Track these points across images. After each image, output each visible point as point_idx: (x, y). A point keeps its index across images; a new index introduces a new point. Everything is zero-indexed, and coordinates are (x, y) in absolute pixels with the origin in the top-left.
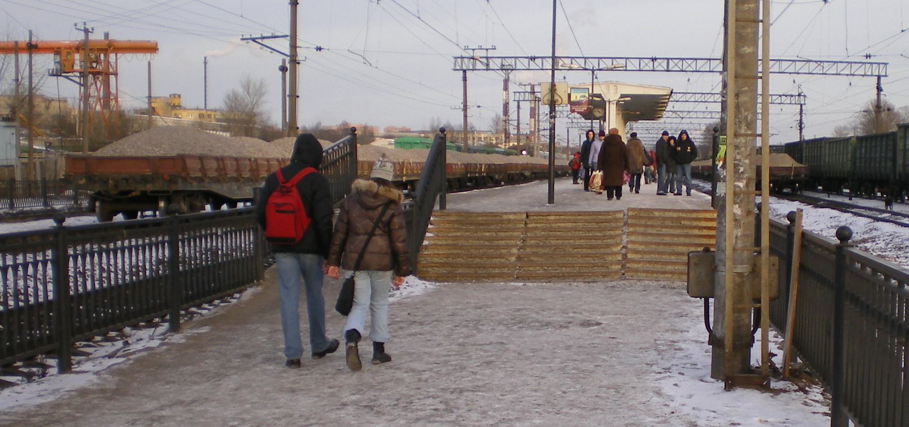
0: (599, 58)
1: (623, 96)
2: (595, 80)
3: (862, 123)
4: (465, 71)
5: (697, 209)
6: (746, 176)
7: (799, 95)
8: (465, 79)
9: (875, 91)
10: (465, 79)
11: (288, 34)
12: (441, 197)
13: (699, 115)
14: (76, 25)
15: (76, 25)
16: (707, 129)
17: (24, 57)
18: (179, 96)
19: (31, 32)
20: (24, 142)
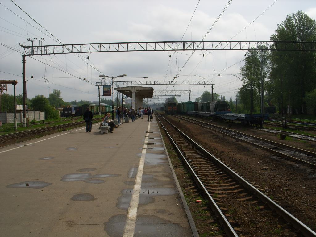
0: (128, 51)
1: (137, 90)
2: (33, 116)
3: (245, 66)
4: (99, 86)
5: (150, 149)
6: (269, 72)
7: (189, 90)
8: (99, 88)
9: (211, 88)
10: (99, 88)
11: (191, 101)
12: (242, 191)
13: (175, 92)
14: (19, 44)
15: (19, 44)
16: (166, 100)
17: (40, 47)
18: (44, 38)
19: (231, 98)
20: (70, 112)
